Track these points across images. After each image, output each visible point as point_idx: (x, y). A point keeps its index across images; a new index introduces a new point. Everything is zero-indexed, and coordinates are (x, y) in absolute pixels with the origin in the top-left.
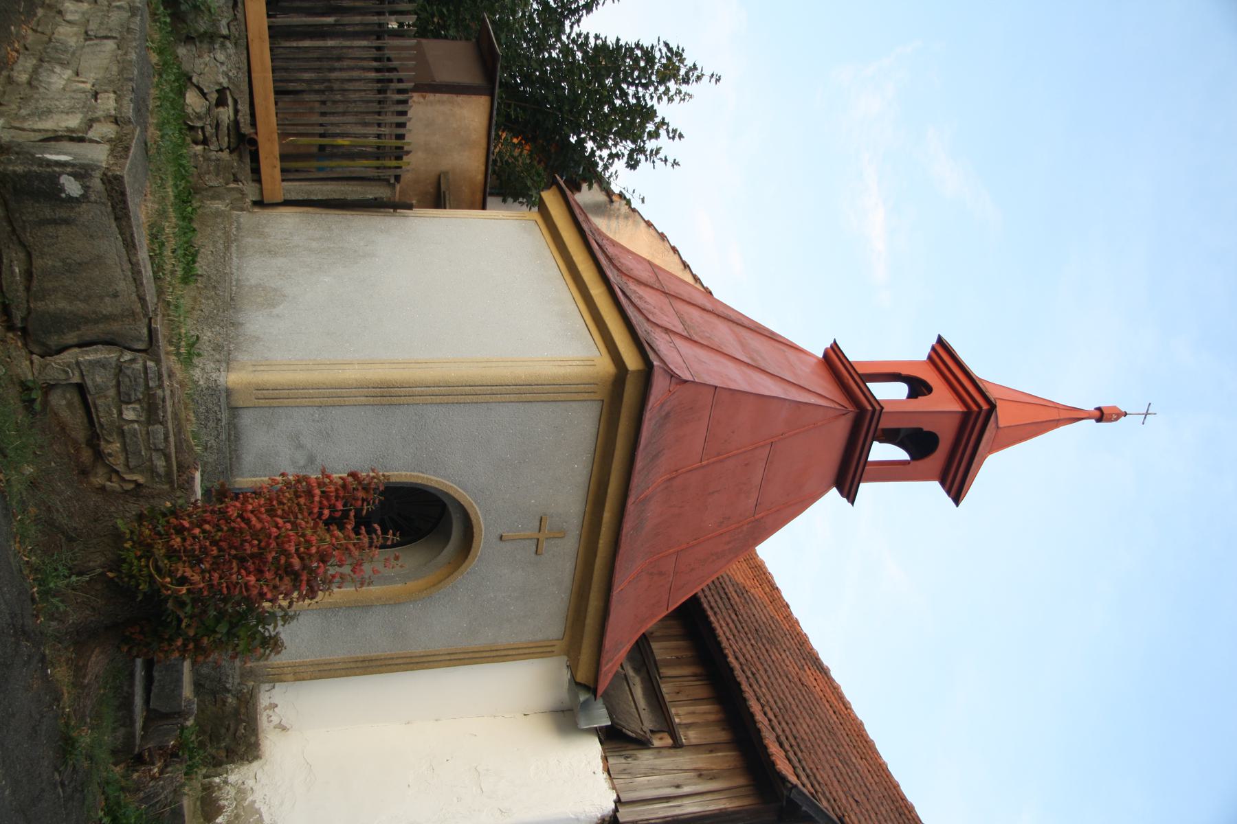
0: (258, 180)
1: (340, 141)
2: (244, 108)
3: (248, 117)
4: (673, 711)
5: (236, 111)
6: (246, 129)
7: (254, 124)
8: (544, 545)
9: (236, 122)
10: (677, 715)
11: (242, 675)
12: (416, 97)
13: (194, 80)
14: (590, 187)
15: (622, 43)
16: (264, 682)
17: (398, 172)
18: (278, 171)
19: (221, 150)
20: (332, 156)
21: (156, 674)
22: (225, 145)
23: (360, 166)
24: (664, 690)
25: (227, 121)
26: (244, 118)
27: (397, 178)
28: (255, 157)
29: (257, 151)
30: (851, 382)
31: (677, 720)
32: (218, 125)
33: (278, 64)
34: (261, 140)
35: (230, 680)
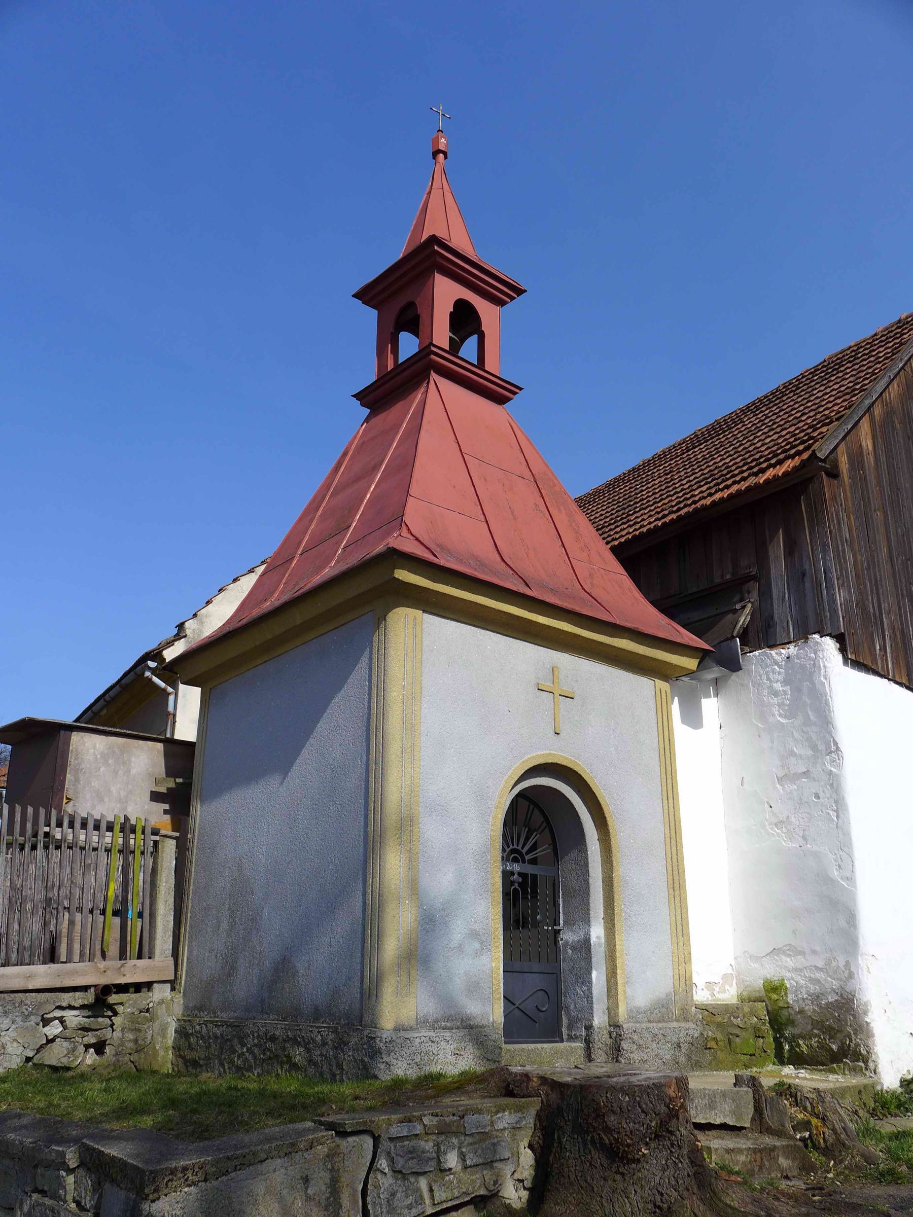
0: (149, 985)
1: (111, 893)
2: (66, 999)
3: (77, 994)
4: (717, 580)
5: (71, 1007)
6: (89, 997)
7: (85, 989)
8: (566, 690)
9: (83, 1007)
10: (722, 576)
11: (686, 1020)
12: (69, 808)
13: (30, 1054)
14: (166, 812)
15: (180, 1017)
16: (692, 996)
17: (148, 831)
18: (140, 963)
19: (112, 1025)
20: (125, 901)
21: (718, 1122)
22: (107, 1021)
23: (140, 879)
24: (695, 590)
25: (80, 1018)
26: (79, 999)
27: (155, 832)
28: (122, 988)
29: (116, 986)
30: (387, 386)
31: (728, 577)
32: (85, 1029)
33: (14, 958)
34: (103, 981)
35: (691, 1032)
